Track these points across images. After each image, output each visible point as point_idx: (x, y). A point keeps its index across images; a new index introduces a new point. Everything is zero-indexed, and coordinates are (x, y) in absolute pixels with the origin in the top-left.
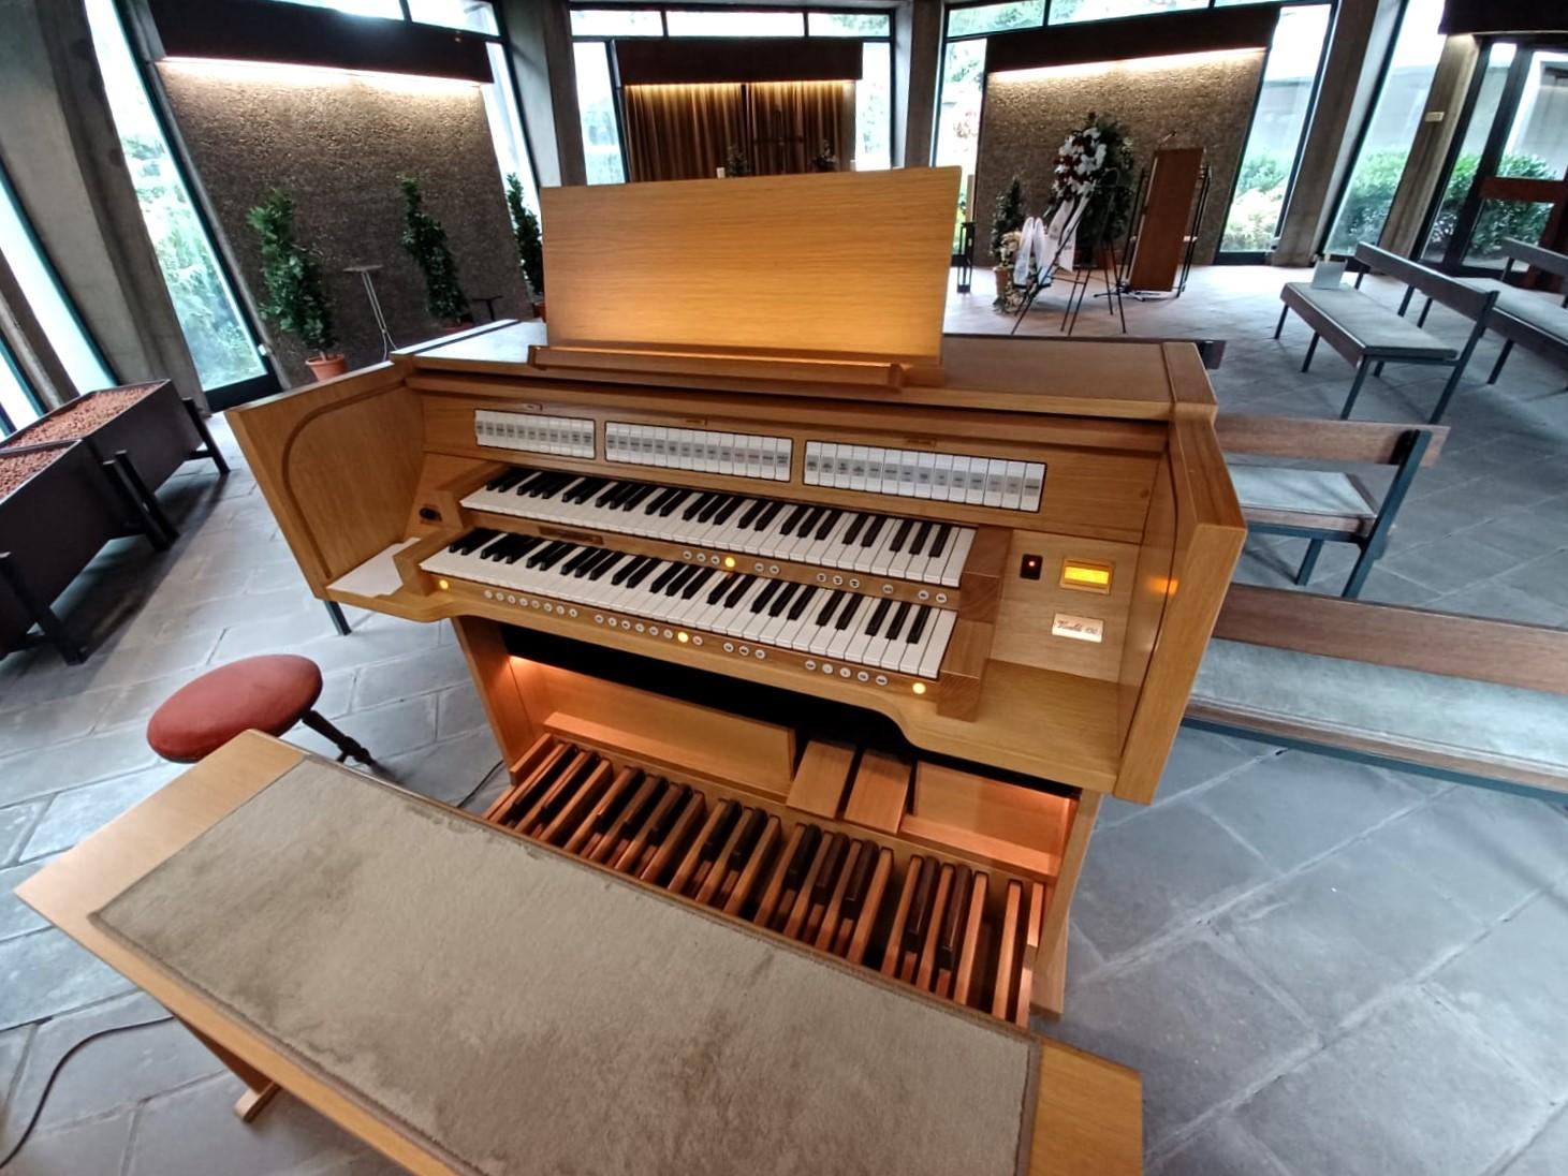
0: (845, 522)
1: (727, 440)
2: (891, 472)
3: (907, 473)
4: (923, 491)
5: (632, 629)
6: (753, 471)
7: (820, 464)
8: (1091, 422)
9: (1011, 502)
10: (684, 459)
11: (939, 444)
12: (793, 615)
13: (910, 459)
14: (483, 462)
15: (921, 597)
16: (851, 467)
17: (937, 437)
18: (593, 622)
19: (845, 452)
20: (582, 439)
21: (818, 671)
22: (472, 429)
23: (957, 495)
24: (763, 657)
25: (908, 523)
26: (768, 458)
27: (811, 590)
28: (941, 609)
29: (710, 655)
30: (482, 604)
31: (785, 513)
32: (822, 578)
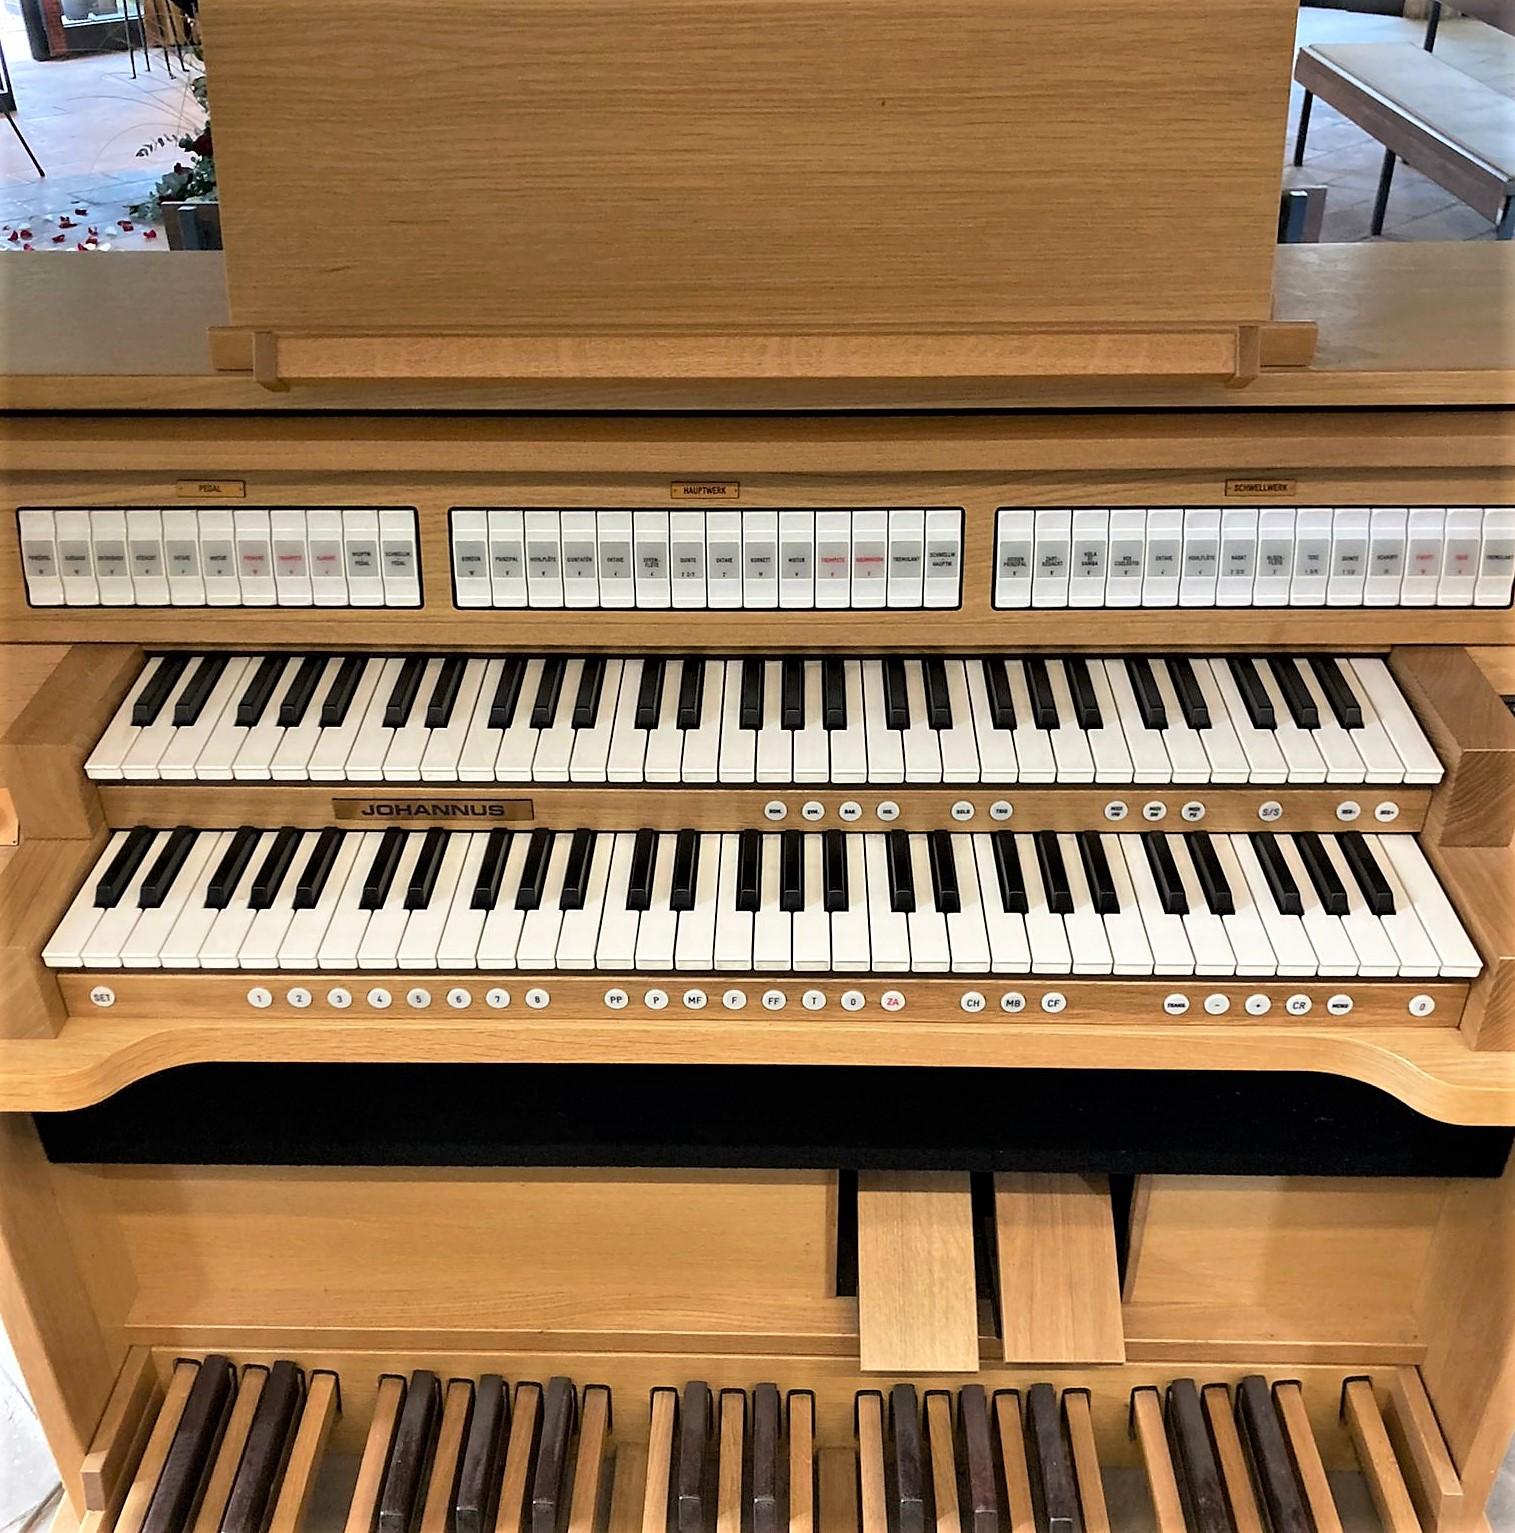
0: (379, 682)
1: (796, 528)
2: (616, 560)
3: (1314, 557)
4: (1271, 593)
5: (833, 1005)
6: (582, 595)
7: (380, 560)
8: (1101, 419)
12: (306, 899)
13: (1241, 526)
14: (64, 650)
16: (1108, 558)
17: (1295, 474)
19: (1091, 527)
20: (380, 560)
21: (1197, 1013)
22: (22, 561)
23: (1344, 593)
25: (415, 662)
26: (906, 559)
27: (184, 839)
28: (616, 833)
31: (237, 678)
32: (1116, 811)
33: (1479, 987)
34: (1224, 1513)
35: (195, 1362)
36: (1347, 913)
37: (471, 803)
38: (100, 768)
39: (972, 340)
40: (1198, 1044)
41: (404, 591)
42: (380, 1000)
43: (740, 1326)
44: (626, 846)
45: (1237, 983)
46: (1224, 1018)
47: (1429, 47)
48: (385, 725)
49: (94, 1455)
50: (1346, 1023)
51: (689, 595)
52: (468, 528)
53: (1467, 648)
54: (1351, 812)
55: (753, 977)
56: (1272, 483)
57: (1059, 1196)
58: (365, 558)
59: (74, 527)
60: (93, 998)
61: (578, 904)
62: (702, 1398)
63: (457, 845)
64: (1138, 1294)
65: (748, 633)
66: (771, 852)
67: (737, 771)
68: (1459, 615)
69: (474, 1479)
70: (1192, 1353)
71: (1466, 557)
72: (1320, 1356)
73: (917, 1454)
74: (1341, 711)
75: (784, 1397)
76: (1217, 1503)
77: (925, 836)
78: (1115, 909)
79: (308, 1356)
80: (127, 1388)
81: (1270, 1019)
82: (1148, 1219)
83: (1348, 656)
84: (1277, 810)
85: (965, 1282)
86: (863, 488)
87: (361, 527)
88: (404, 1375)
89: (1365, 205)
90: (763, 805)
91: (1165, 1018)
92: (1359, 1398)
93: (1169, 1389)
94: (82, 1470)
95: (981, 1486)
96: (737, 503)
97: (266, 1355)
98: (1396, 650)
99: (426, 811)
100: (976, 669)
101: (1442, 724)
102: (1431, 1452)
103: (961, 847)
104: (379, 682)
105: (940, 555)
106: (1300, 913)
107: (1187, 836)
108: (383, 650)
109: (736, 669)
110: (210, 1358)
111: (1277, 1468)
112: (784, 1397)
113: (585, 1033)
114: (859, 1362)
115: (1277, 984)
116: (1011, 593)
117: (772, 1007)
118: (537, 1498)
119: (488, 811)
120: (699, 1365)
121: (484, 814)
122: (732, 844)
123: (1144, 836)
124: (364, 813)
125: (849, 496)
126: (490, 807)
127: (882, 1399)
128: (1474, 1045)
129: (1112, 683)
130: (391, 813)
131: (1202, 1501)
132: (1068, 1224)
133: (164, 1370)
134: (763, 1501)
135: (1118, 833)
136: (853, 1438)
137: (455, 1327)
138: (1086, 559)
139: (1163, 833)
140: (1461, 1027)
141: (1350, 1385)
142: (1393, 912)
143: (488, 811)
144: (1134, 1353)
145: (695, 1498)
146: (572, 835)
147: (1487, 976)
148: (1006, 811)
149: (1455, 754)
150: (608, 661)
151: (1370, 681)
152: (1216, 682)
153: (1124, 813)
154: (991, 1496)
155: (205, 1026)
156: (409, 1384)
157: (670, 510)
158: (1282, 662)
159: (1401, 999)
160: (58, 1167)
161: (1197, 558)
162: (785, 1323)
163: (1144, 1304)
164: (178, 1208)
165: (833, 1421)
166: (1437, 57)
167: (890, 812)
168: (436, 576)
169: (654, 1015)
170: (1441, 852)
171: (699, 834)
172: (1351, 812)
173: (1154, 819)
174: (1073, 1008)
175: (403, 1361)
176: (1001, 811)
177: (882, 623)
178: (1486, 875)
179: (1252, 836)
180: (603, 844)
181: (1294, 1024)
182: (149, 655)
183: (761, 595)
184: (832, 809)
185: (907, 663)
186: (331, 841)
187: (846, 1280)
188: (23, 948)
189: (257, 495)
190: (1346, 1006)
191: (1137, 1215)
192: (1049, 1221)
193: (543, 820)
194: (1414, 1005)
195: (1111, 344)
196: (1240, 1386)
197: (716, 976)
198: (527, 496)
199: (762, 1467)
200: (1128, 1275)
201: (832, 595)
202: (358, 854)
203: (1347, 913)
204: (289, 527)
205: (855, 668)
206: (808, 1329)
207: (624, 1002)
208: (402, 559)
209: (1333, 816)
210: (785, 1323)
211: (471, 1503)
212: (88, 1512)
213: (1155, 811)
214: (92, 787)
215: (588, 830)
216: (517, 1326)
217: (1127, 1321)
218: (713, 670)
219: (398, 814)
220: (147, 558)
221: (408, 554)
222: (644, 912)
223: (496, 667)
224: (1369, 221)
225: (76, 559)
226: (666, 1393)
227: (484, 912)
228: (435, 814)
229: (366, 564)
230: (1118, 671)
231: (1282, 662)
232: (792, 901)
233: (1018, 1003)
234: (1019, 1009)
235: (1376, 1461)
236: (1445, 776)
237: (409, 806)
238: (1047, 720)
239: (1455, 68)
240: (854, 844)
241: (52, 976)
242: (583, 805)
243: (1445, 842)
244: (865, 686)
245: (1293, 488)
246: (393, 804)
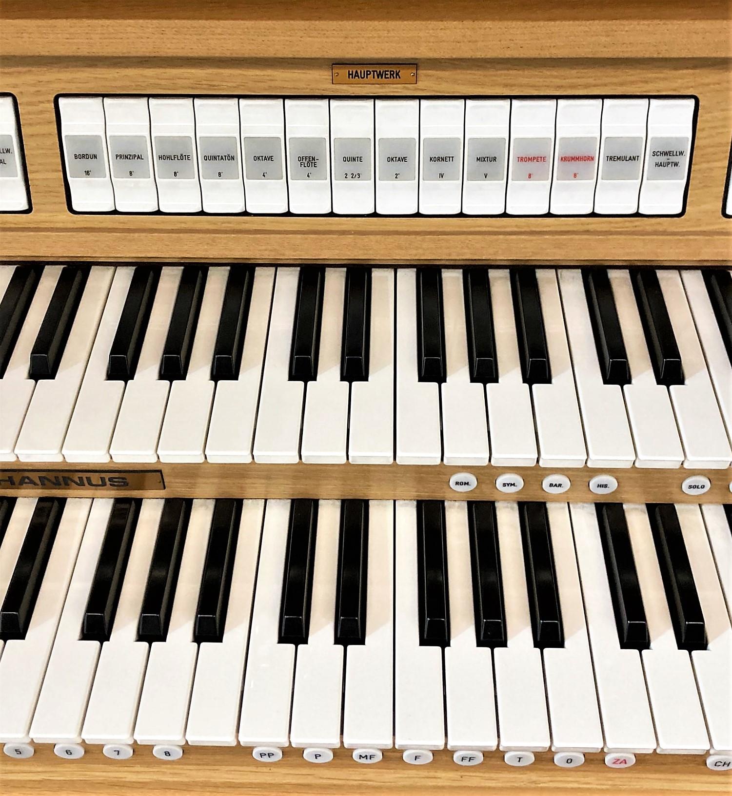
34: (604, 237)
37: (88, 475)
65: (425, 245)
86: (574, 72)
90: (449, 476)
96: (416, 89)
105: (666, 154)
109: (408, 280)
119: (108, 483)
125: (558, 82)
126: (110, 479)
143: (108, 483)
150: (257, 268)
157: (330, 98)
161: (169, 157)
172: (606, 486)
198: (152, 81)
221: (8, 151)
222: (300, 647)
227: (96, 643)
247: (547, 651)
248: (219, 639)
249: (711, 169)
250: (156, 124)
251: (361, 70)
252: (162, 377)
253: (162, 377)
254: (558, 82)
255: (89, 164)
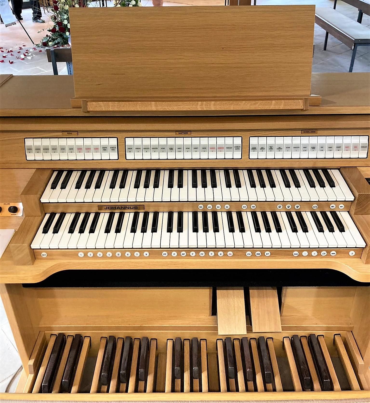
1: (204, 141)
4: (313, 155)
7: (109, 149)
9: (354, 155)
10: (37, 154)
11: (319, 132)
12: (56, 231)
13: (305, 140)
15: (200, 208)
18: (245, 256)
19: (271, 141)
21: (300, 256)
22: (24, 150)
24: (148, 255)
25: (116, 172)
29: (237, 260)
30: (77, 261)
32: (280, 207)
33: (365, 249)
35: (55, 335)
36: (334, 232)
38: (44, 200)
39: (244, 102)
40: (301, 263)
41: (114, 156)
42: (109, 255)
43: (189, 324)
44: (166, 215)
45: (310, 249)
46: (307, 257)
47: (335, 8)
48: (110, 188)
49: (31, 360)
50: (335, 257)
51: (180, 156)
52: (129, 142)
53: (357, 167)
54: (333, 207)
55: (197, 249)
56: (312, 131)
57: (265, 290)
58: (105, 149)
59: (38, 142)
60: (42, 255)
61: (156, 231)
62: (179, 341)
63: (126, 216)
64: (284, 314)
66: (200, 216)
67: (192, 198)
68: (355, 160)
69: (124, 364)
70: (297, 328)
71: (356, 147)
72: (328, 329)
73: (232, 355)
74: (330, 183)
75: (199, 341)
76: (305, 367)
77: (236, 212)
78: (281, 231)
79: (84, 333)
80: (39, 342)
81: (317, 257)
82: (286, 296)
83: (330, 169)
84: (316, 206)
85: (243, 312)
87: (105, 142)
88: (107, 337)
89: (322, 43)
91: (293, 257)
92: (338, 339)
93: (292, 337)
94: (28, 364)
95: (248, 364)
97: (73, 333)
98: (342, 168)
99: (119, 208)
100: (245, 172)
101: (354, 187)
102: (356, 353)
103: (244, 215)
104: (108, 177)
105: (237, 147)
106: (323, 232)
107: (296, 212)
108: (109, 169)
109: (190, 172)
110: (60, 334)
111: (319, 358)
112: (199, 341)
113: (157, 262)
114: (218, 332)
115: (319, 250)
116: (253, 155)
117: (202, 255)
118: (140, 369)
120: (179, 333)
121: (133, 208)
122: (191, 215)
123: (286, 212)
124: (105, 209)
125: (217, 134)
127: (223, 341)
128: (365, 263)
129: (277, 176)
130: (111, 209)
131: (302, 367)
132: (267, 297)
133: (48, 337)
134: (195, 368)
135: (280, 212)
136: (216, 351)
137: (120, 325)
138: (270, 148)
139: (291, 212)
140: (361, 258)
141: (335, 336)
142: (344, 231)
144: (284, 329)
145: (179, 368)
146: (153, 213)
147: (367, 247)
148: (254, 207)
149: (357, 194)
151: (336, 175)
152: (301, 176)
153: (282, 207)
154: (251, 366)
155: (68, 262)
156: (108, 339)
157: (175, 137)
158: (315, 171)
159: (347, 252)
160: (24, 288)
162: (200, 323)
163: (286, 316)
164: (53, 296)
165: (211, 346)
166: (337, 11)
167: (227, 207)
168: (122, 153)
169: (174, 258)
170: (354, 216)
171: (183, 212)
172: (333, 207)
173: (288, 208)
174: (272, 255)
175: (106, 333)
176: (253, 207)
177: (224, 162)
178: (365, 222)
179: (311, 212)
180: (160, 215)
181: (323, 258)
182: (54, 171)
183: (196, 156)
184: (214, 206)
185: (229, 171)
186: (97, 215)
187: (214, 312)
188: (26, 245)
189: (80, 135)
190: (335, 254)
191: (283, 295)
192: (263, 296)
193: (146, 210)
194: (350, 253)
195: (275, 103)
196: (309, 336)
197: (188, 249)
199: (195, 359)
200: (282, 308)
201: (212, 156)
202: (104, 218)
203: (334, 232)
204: (88, 142)
205: (218, 172)
206: (206, 324)
207: (167, 255)
208: (238, 148)
209: (329, 208)
210: (200, 323)
211: (124, 371)
212: (30, 374)
213: (289, 207)
214: (42, 204)
215: (157, 212)
216: (135, 325)
217: (282, 320)
218: (185, 172)
219: (113, 209)
220: (54, 149)
222: (171, 233)
223: (135, 173)
224: (323, 47)
225: (38, 149)
226: (171, 340)
228: (121, 209)
229: (106, 150)
230: (278, 173)
231: (315, 171)
232: (206, 230)
233: (259, 254)
234: (260, 255)
235: (343, 356)
236: (355, 199)
237: (115, 207)
238: (263, 185)
239: (342, 14)
240: (219, 214)
241: (32, 250)
242: (155, 206)
243: (355, 214)
244: (220, 177)
245: (317, 132)
246: (112, 207)
247: (216, 233)
248: (156, 232)
249: (246, 150)
250: (366, 141)
251: (181, 132)
252: (144, 188)
253: (144, 188)
254: (217, 134)
255: (30, 151)
